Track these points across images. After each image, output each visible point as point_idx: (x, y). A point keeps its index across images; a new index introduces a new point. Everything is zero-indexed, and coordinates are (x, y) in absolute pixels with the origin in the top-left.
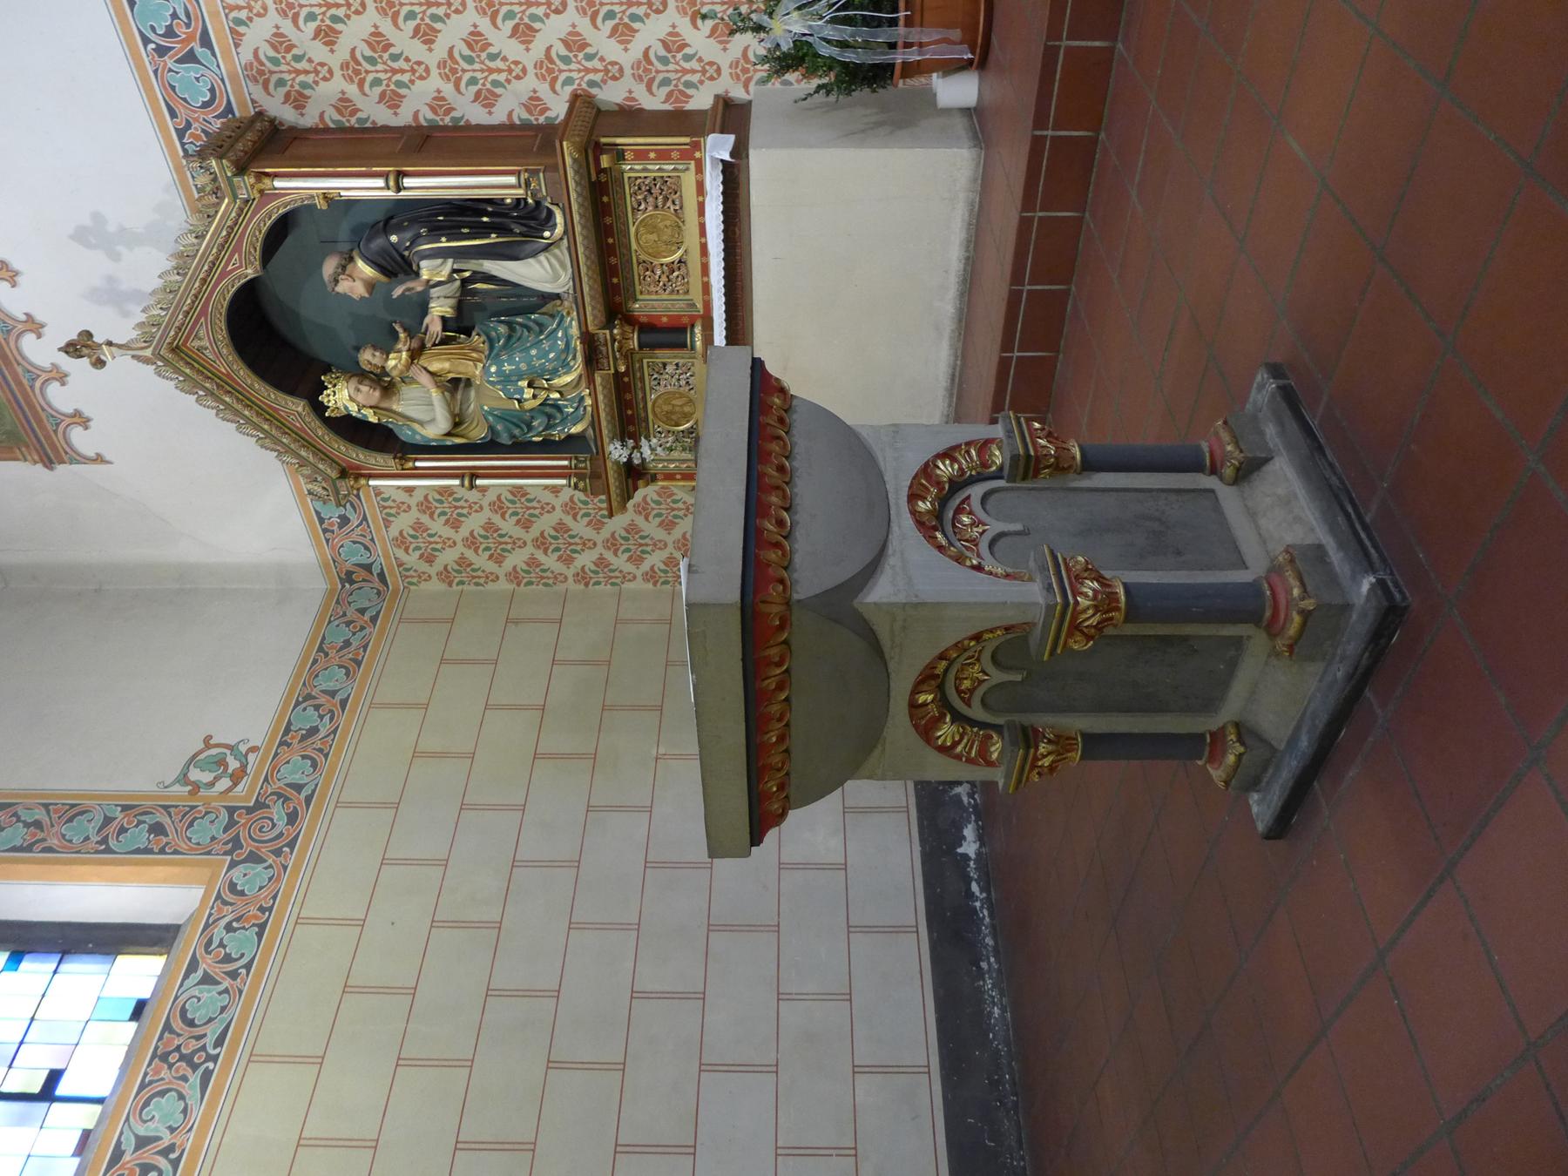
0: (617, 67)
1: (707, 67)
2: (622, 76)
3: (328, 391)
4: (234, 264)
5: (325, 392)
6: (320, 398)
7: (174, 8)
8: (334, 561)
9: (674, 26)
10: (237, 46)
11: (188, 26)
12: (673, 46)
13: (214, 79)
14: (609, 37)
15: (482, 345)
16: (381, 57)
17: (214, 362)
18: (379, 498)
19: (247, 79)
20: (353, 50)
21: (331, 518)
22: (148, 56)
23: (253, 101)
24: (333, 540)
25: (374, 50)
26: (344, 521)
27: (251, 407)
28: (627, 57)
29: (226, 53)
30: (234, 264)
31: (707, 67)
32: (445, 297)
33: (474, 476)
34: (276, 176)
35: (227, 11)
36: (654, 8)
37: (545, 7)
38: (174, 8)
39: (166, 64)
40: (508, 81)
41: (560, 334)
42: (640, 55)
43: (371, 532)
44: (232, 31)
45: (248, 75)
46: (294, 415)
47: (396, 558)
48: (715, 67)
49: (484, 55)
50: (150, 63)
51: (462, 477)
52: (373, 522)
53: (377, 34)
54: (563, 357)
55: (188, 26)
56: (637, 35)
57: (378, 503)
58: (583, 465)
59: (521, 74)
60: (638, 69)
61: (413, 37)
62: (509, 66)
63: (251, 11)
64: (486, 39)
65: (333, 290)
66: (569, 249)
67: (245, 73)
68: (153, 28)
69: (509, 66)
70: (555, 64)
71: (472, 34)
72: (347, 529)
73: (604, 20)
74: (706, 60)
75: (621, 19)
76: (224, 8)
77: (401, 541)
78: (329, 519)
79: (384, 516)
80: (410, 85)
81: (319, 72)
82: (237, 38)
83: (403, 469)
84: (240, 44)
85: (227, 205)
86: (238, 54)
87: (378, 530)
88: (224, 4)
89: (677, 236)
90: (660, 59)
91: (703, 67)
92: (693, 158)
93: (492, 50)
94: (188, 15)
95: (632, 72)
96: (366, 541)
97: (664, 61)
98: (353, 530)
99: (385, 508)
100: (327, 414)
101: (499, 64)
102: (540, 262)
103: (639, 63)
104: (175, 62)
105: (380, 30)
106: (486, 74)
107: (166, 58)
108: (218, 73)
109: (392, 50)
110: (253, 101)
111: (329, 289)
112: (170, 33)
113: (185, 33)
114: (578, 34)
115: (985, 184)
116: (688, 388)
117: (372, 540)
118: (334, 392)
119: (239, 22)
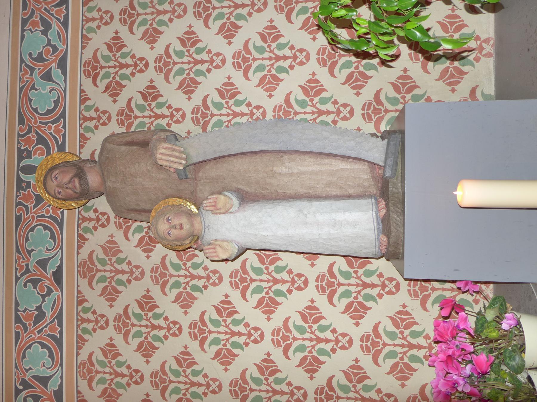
16: (184, 371)
18: (80, 308)
19: (82, 73)
20: (164, 363)
23: (79, 392)
25: (106, 357)
35: (79, 323)
37: (246, 337)
44: (81, 135)
49: (189, 371)
53: (186, 353)
56: (86, 343)
59: (217, 389)
61: (136, 351)
62: (208, 382)
68: (30, 55)
69: (208, 382)
71: (264, 360)
73: (133, 337)
80: (203, 396)
81: (133, 377)
82: (81, 341)
86: (82, 53)
99: (83, 320)
106: (188, 386)
109: (195, 367)
110: (79, 392)
119: (85, 331)
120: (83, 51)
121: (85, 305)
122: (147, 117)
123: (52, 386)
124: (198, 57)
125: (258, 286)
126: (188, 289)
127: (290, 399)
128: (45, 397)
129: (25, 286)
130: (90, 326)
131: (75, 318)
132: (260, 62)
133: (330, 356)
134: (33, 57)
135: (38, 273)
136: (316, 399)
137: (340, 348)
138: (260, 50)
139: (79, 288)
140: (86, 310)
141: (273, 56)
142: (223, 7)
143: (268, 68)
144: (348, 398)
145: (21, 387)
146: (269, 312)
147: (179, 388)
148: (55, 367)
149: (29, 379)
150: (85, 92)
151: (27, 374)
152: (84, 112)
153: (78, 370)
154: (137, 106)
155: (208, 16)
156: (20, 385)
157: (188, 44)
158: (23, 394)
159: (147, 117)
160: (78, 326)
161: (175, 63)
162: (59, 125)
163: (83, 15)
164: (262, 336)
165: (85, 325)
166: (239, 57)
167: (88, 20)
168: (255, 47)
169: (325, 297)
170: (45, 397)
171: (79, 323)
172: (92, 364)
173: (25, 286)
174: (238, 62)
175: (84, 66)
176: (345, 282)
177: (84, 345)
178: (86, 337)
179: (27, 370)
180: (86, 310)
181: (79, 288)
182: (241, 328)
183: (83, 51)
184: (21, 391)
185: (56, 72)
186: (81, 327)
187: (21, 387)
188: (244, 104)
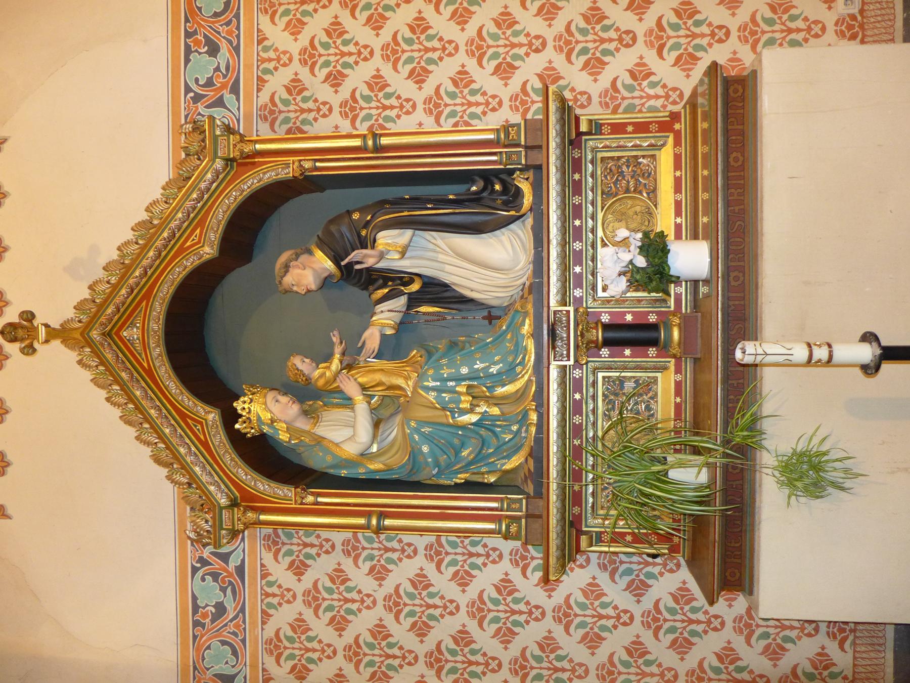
0: (586, 96)
1: (671, 93)
2: (589, 104)
3: (246, 399)
4: (194, 240)
5: (242, 399)
6: (235, 404)
7: (219, 63)
8: (195, 668)
9: (641, 58)
10: (259, 90)
11: (225, 76)
12: (640, 75)
13: (231, 118)
14: (581, 70)
15: (419, 359)
17: (139, 354)
18: (264, 582)
19: (262, 548)
21: (207, 605)
22: (185, 103)
24: (202, 636)
26: (221, 609)
27: (160, 410)
28: (595, 87)
29: (248, 96)
30: (194, 240)
31: (671, 93)
32: (389, 311)
33: (382, 516)
34: (263, 511)
36: (625, 42)
38: (219, 63)
39: (197, 108)
40: (484, 113)
41: (509, 337)
42: (608, 85)
43: (245, 629)
44: (263, 611)
45: (260, 115)
46: (201, 423)
47: (264, 670)
48: (678, 92)
50: (185, 109)
51: (368, 515)
52: (250, 617)
54: (510, 359)
55: (225, 76)
57: (262, 588)
58: (518, 505)
60: (606, 96)
63: (279, 62)
64: (471, 77)
65: (280, 283)
66: (533, 228)
67: (265, 646)
68: (197, 80)
70: (444, 655)
72: (220, 623)
74: (670, 86)
75: (594, 54)
76: (262, 595)
77: (275, 646)
78: (204, 608)
79: (264, 607)
83: (302, 504)
84: (262, 89)
85: (207, 163)
86: (257, 97)
87: (253, 624)
88: (263, 592)
89: (647, 223)
90: (626, 87)
91: (667, 93)
92: (671, 130)
93: (474, 86)
94: (227, 69)
95: (600, 100)
96: (236, 642)
97: (630, 88)
98: (226, 625)
99: (268, 595)
100: (237, 426)
101: (479, 98)
102: (501, 241)
103: (607, 91)
104: (205, 107)
105: (381, 73)
107: (199, 104)
108: (237, 114)
111: (278, 279)
112: (209, 83)
113: (221, 83)
114: (554, 69)
115: (761, 460)
116: (647, 414)
117: (244, 641)
118: (251, 400)
119: (270, 605)
120: (259, 94)
121: (270, 578)
122: (332, 55)
123: (234, 562)
124: (387, 103)
125: (453, 559)
126: (380, 10)
127: (661, 681)
128: (225, 574)
129: (203, 580)
130: (275, 601)
131: (261, 669)
132: (452, 108)
133: (523, 627)
134: (200, 83)
135: (217, 566)
136: (687, 681)
137: (534, 620)
138: (452, 96)
139: (264, 666)
140: (270, 584)
141: (465, 102)
142: (412, 51)
143: (460, 114)
144: (719, 680)
145: (198, 565)
146: (464, 585)
147: (374, 661)
148: (240, 664)
149: (209, 557)
150: (267, 671)
151: (205, 551)
152: (265, 588)
153: (259, 6)
154: (321, 43)
155: (397, 60)
156: (197, 562)
157: (376, 88)
158: (200, 574)
159: (332, 55)
160: (262, 601)
161: (362, 109)
162: (239, 621)
163: (258, 55)
164: (458, 608)
165: (270, 600)
166: (430, 103)
167: (264, 61)
168: (447, 92)
169: (519, 570)
170: (225, 574)
171: (263, 597)
172: (280, 641)
173: (203, 580)
174: (429, 108)
175: (266, 644)
176: (453, 551)
177: (269, 620)
178: (271, 611)
179: (208, 669)
180: (270, 584)
181: (264, 666)
182: (437, 601)
183: (259, 94)
184: (198, 569)
185: (228, 98)
186: (265, 602)
187: (198, 565)
188: (436, 39)
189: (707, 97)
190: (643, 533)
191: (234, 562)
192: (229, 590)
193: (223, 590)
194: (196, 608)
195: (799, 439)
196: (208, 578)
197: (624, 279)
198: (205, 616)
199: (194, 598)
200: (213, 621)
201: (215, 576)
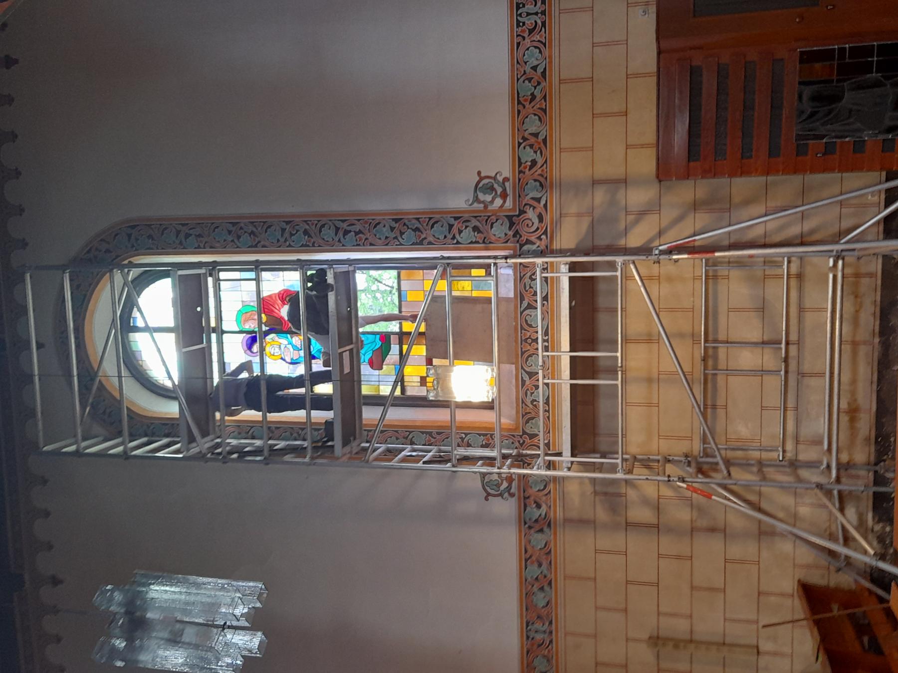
21: (526, 162)
78: (525, 163)
158: (523, 145)
184: (521, 143)
189: (126, 270)
190: (847, 137)
191: (541, 138)
192: (539, 152)
193: (535, 152)
194: (520, 164)
195: (792, 643)
196: (528, 148)
197: (567, 266)
198: (525, 168)
199: (519, 159)
200: (529, 170)
201: (531, 146)
